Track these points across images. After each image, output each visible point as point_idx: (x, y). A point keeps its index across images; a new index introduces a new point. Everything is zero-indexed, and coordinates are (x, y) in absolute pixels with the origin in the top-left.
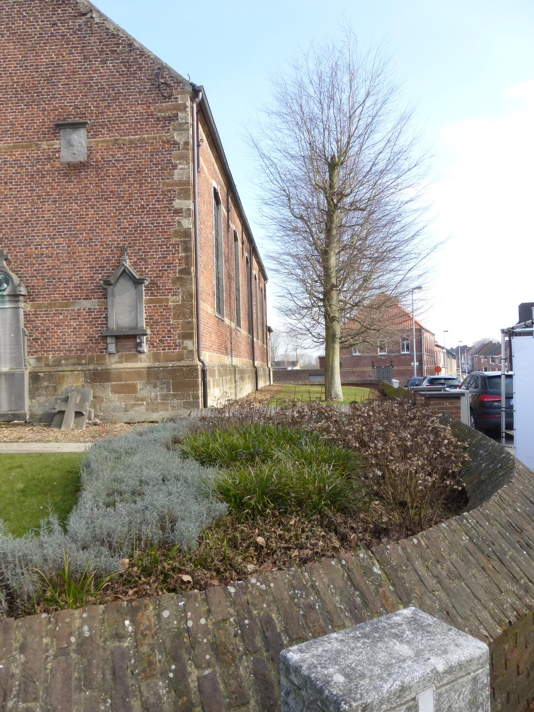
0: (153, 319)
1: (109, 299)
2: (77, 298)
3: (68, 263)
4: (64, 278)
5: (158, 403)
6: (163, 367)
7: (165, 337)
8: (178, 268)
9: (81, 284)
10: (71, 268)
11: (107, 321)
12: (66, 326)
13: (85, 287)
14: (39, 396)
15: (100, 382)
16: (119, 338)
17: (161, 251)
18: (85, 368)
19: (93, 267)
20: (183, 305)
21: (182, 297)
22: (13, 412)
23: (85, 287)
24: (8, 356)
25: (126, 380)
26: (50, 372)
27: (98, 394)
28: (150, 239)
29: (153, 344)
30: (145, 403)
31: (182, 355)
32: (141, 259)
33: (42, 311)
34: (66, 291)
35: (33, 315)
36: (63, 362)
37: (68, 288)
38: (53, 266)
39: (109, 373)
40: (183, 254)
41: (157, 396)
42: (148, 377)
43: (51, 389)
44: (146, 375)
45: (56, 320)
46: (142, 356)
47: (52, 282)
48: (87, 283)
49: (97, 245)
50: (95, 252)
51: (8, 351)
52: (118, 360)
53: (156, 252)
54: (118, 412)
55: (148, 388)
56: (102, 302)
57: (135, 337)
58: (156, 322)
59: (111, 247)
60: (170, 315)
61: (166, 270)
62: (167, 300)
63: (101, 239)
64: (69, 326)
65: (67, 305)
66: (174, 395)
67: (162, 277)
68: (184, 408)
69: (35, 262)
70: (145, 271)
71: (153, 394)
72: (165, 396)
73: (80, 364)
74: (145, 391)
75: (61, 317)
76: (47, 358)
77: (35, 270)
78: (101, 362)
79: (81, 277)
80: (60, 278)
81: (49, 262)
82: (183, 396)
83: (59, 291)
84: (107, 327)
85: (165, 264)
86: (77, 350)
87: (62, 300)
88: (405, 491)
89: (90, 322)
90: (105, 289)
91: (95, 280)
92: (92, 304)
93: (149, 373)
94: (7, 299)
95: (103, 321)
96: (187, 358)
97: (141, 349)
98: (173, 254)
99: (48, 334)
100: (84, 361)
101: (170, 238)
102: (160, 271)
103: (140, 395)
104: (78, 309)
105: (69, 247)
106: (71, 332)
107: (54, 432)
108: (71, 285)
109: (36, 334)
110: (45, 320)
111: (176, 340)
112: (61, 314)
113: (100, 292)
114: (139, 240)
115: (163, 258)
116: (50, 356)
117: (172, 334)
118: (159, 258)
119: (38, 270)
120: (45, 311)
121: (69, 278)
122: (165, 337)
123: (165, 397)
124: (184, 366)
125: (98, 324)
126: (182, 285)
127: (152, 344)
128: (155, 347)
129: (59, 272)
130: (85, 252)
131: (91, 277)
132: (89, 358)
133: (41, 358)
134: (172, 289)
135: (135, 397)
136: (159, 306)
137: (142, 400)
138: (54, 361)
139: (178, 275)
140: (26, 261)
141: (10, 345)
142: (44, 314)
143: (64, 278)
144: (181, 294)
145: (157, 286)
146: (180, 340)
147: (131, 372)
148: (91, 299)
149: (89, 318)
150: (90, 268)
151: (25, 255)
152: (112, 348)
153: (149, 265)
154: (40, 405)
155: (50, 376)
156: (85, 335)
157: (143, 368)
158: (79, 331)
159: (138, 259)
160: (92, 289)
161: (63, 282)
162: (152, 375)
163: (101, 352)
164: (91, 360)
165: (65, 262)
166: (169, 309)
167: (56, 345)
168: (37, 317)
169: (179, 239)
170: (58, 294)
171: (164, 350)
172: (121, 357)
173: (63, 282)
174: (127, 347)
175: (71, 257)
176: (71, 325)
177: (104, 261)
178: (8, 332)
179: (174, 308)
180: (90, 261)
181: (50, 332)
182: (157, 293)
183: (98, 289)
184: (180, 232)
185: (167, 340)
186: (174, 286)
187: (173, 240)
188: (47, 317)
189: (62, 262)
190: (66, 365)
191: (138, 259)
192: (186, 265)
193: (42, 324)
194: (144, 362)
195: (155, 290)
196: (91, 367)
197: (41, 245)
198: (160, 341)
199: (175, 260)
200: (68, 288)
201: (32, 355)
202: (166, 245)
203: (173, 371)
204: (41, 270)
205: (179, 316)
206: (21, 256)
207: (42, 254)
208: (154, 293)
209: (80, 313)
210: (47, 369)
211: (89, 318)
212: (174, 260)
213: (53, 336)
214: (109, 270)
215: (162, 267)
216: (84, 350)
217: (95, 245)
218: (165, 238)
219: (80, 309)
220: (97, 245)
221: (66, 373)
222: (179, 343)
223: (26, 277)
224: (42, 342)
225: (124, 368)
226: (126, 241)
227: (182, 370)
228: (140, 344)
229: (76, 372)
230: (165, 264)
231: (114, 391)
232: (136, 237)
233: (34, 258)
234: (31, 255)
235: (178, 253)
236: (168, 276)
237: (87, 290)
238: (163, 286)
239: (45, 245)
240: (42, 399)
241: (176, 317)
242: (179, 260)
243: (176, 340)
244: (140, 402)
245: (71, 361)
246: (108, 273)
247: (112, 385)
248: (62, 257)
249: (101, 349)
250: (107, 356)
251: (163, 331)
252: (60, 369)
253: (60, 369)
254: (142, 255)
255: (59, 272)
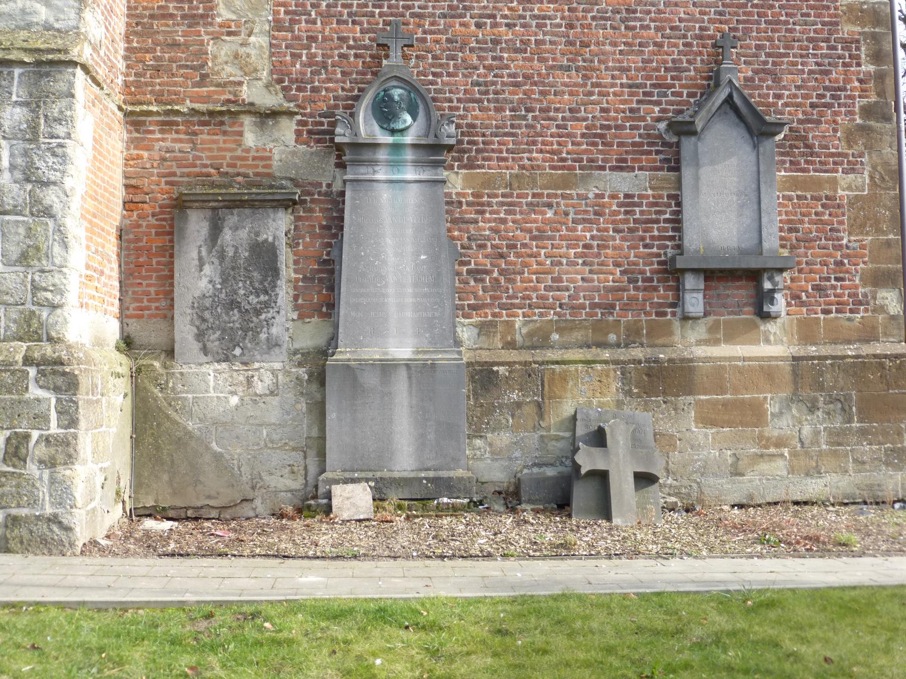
0: (797, 230)
1: (687, 173)
2: (593, 165)
3: (568, 69)
4: (557, 110)
5: (820, 453)
6: (834, 358)
7: (828, 279)
8: (859, 103)
9: (603, 127)
10: (576, 85)
11: (678, 229)
12: (562, 238)
13: (616, 136)
14: (493, 431)
15: (665, 393)
16: (715, 276)
17: (815, 55)
18: (623, 354)
19: (638, 86)
20: (872, 199)
21: (872, 178)
22: (431, 474)
23: (616, 136)
24: (409, 314)
25: (736, 391)
26: (526, 364)
27: (663, 427)
28: (786, 23)
29: (799, 297)
30: (786, 452)
31: (874, 328)
32: (764, 71)
33: (496, 196)
34: (564, 144)
35: (469, 204)
36: (555, 337)
37: (568, 135)
38: (525, 76)
39: (692, 370)
40: (872, 68)
41: (817, 433)
42: (795, 383)
43: (529, 410)
44: (788, 377)
45: (535, 221)
46: (771, 327)
47: (524, 118)
48: (624, 128)
49: (648, 27)
50: (641, 45)
51: (409, 300)
52: (705, 336)
53: (802, 56)
54: (715, 475)
55: (794, 411)
56: (664, 179)
57: (754, 276)
58: (807, 241)
59: (685, 37)
60: (841, 223)
61: (828, 106)
62: (834, 182)
63: (659, 12)
64: (572, 241)
65: (566, 183)
66: (863, 432)
67: (818, 122)
68: (887, 464)
69: (475, 61)
70: (775, 104)
71: (807, 430)
72: (838, 435)
73: (602, 345)
74: (786, 421)
75: (550, 214)
76: (510, 325)
77: (478, 84)
78: (660, 341)
79: (603, 110)
80: (548, 110)
81: (517, 64)
82: (885, 433)
83: (543, 143)
84: (679, 247)
85: (826, 88)
86: (593, 306)
87: (552, 168)
88: (118, 655)
89: (631, 230)
90: (672, 148)
91: (643, 119)
92: (636, 182)
93: (795, 373)
94: (409, 155)
95: (665, 230)
96: (885, 334)
97: (773, 309)
98: (845, 65)
99: (512, 258)
100: (612, 338)
101: (837, 24)
102: (813, 105)
103: (772, 431)
104: (597, 196)
105: (571, 26)
106: (576, 255)
107: (584, 532)
108: (579, 129)
109: (480, 259)
110: (503, 221)
111: (856, 287)
112: (550, 206)
113: (658, 152)
114: (758, 23)
115: (822, 72)
116: (518, 321)
117: (847, 272)
118: (811, 72)
119: (486, 84)
120: (503, 196)
121: (571, 110)
122: (828, 279)
123: (837, 438)
124: (886, 356)
125: (653, 238)
126: (869, 147)
127: (797, 297)
128: (802, 304)
129: (542, 93)
130: (614, 44)
131: (632, 110)
132: (627, 329)
133: (492, 324)
134: (846, 155)
135: (761, 437)
136: (813, 198)
137: (780, 443)
138: (530, 335)
139: (859, 121)
140: (453, 58)
141: (416, 285)
142: (502, 204)
143: (557, 110)
144: (868, 168)
145: (807, 146)
146: (867, 289)
147: (751, 369)
148: (632, 169)
149: (626, 221)
150: (630, 86)
151: (449, 41)
152: (694, 302)
153: (785, 88)
154: (496, 454)
155: (529, 375)
156: (617, 264)
157: (782, 359)
158: (598, 255)
159: (756, 72)
160: (634, 144)
161: (554, 119)
162: (805, 379)
163: (658, 314)
164: (632, 336)
165: (561, 68)
166: (839, 206)
167: (535, 289)
168: (482, 212)
169: (859, 29)
170: (541, 151)
171: (826, 312)
172: (713, 329)
173: (554, 119)
174: (729, 300)
175: (577, 54)
176: (578, 239)
177: (667, 70)
178: (409, 249)
179: (851, 204)
180: (628, 69)
181: (518, 255)
182: (807, 162)
183: (649, 144)
184: (862, 11)
185: (834, 287)
186: (850, 147)
187: (848, 29)
188: (508, 212)
189: (552, 67)
190: (565, 347)
191: (756, 72)
192: (878, 95)
193: (495, 231)
194: (776, 343)
195: (803, 155)
196: (638, 353)
197: (493, 17)
198: (816, 288)
199: (849, 81)
200: (568, 135)
201: (466, 316)
202: (827, 40)
203: (859, 368)
204: (494, 83)
205: (862, 226)
206: (437, 42)
207: (496, 42)
208: (799, 163)
209: (603, 206)
210: (513, 356)
211: (626, 221)
212: (847, 81)
213: (525, 265)
214: (680, 94)
215: (820, 96)
216: (613, 307)
217: (642, 27)
218: (824, 24)
219: (602, 196)
220: (648, 27)
221: (572, 368)
222: (865, 295)
223: (451, 101)
224: (496, 280)
225: (730, 359)
226: (726, 22)
227: (882, 365)
228: (770, 296)
229: (599, 367)
230: (826, 88)
231: (706, 421)
232: (750, 14)
233: (472, 50)
234: (465, 43)
235: (859, 65)
236: (835, 122)
237: (620, 144)
238: (821, 147)
239: (505, 17)
240: (503, 439)
241: (858, 227)
242: (861, 81)
243: (856, 287)
244: (772, 450)
245: (578, 335)
246: (679, 103)
247: (699, 403)
248: (553, 52)
249: (661, 305)
250: (677, 324)
251: (824, 263)
252: (551, 355)
253: (551, 355)
254: (765, 63)
255: (542, 93)
